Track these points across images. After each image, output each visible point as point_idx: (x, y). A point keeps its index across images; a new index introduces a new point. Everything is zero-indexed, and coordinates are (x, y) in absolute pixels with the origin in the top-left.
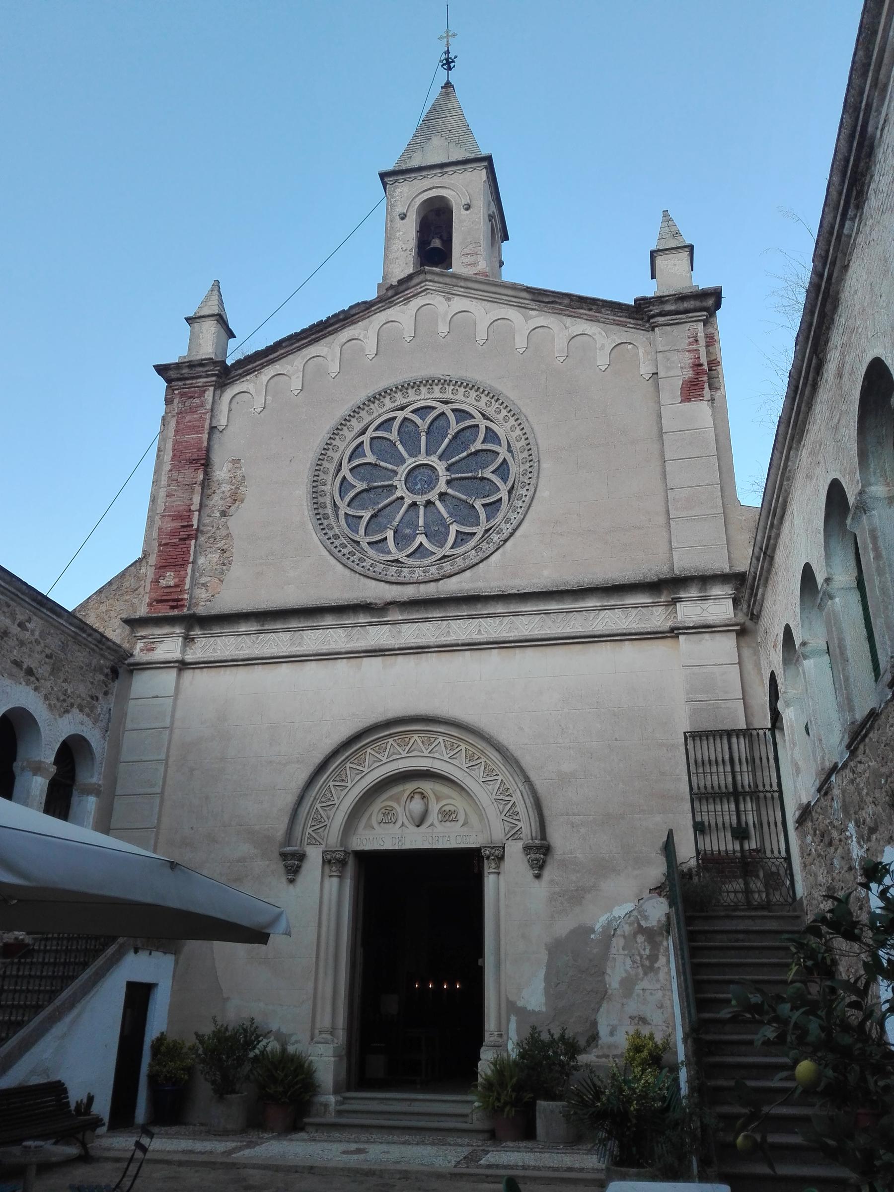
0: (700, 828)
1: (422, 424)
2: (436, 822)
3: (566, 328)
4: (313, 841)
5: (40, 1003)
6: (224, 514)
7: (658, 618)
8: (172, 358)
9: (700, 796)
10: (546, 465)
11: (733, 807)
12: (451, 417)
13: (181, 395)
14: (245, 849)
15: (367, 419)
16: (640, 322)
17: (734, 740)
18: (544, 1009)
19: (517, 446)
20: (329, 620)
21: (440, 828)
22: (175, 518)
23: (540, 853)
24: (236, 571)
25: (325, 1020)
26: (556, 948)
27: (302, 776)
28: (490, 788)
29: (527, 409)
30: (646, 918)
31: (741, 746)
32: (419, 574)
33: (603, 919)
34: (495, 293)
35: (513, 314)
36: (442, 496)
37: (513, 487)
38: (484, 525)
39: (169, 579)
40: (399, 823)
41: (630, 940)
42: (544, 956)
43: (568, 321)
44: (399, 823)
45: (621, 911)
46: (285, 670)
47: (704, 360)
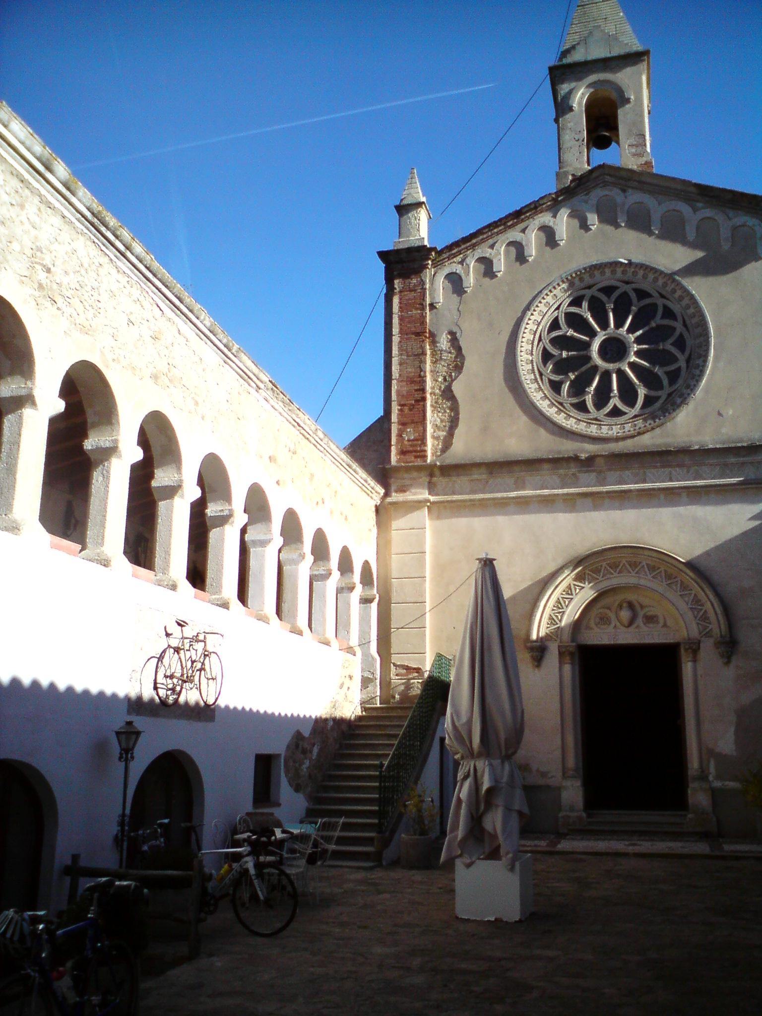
2: (642, 624)
3: (730, 219)
5: (68, 880)
8: (388, 247)
12: (633, 295)
18: (734, 753)
21: (644, 629)
23: (729, 646)
25: (571, 762)
28: (686, 599)
35: (684, 208)
36: (632, 366)
37: (690, 355)
38: (667, 389)
40: (612, 625)
43: (731, 213)
44: (612, 625)
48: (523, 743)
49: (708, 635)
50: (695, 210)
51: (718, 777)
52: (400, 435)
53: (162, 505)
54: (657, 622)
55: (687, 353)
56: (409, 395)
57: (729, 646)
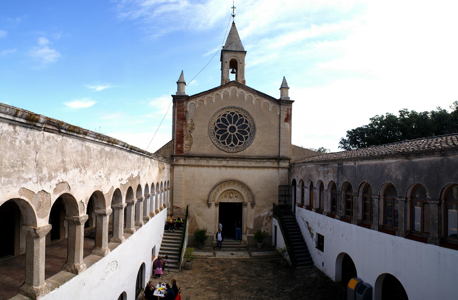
0: (279, 201)
1: (233, 116)
4: (213, 201)
6: (189, 132)
7: (276, 165)
9: (280, 196)
10: (258, 131)
13: (178, 102)
14: (200, 201)
15: (221, 113)
16: (177, 271)
19: (252, 125)
20: (214, 159)
21: (235, 199)
22: (180, 132)
23: (253, 205)
24: (193, 146)
26: (255, 220)
27: (210, 189)
29: (254, 117)
32: (232, 150)
34: (233, 244)
35: (252, 95)
36: (237, 134)
38: (245, 141)
39: (179, 146)
41: (267, 218)
42: (253, 220)
43: (264, 99)
45: (266, 214)
46: (205, 168)
48: (252, 189)
50: (255, 96)
51: (249, 234)
53: (35, 241)
56: (179, 135)
57: (253, 205)
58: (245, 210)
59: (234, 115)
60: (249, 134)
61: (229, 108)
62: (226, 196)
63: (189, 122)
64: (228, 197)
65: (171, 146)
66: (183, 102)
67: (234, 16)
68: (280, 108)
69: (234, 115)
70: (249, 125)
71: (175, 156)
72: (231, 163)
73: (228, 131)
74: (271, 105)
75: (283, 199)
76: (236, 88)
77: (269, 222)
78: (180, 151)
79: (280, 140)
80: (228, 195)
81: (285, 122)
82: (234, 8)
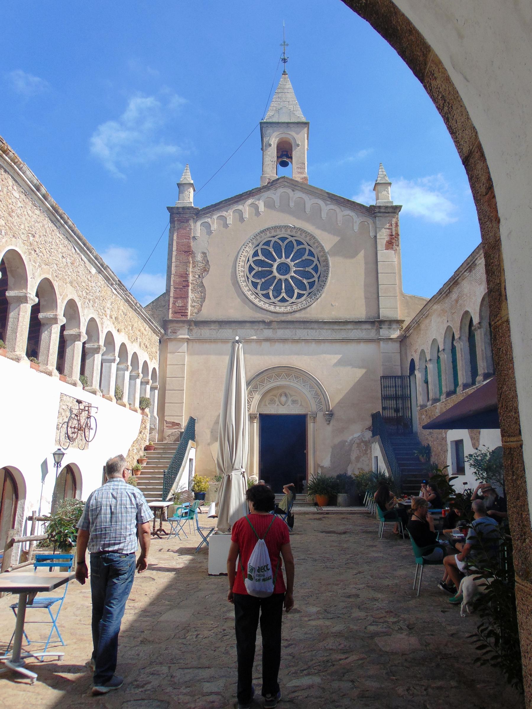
2: (290, 404)
7: (372, 334)
9: (385, 398)
11: (395, 401)
13: (178, 220)
17: (397, 379)
30: (364, 438)
31: (399, 382)
33: (350, 438)
35: (321, 202)
41: (359, 445)
42: (331, 450)
45: (356, 435)
47: (394, 233)
49: (321, 410)
50: (327, 205)
52: (174, 303)
54: (298, 403)
55: (319, 274)
58: (311, 427)
59: (286, 242)
60: (316, 276)
61: (275, 228)
62: (272, 401)
63: (199, 257)
64: (277, 403)
65: (163, 304)
66: (188, 221)
67: (284, 61)
68: (374, 223)
69: (286, 242)
70: (315, 260)
71: (172, 321)
72: (281, 333)
73: (275, 273)
74: (357, 220)
75: (392, 403)
76: (289, 191)
77: (366, 453)
78: (182, 311)
79: (378, 285)
80: (277, 399)
81: (387, 249)
82: (285, 44)
